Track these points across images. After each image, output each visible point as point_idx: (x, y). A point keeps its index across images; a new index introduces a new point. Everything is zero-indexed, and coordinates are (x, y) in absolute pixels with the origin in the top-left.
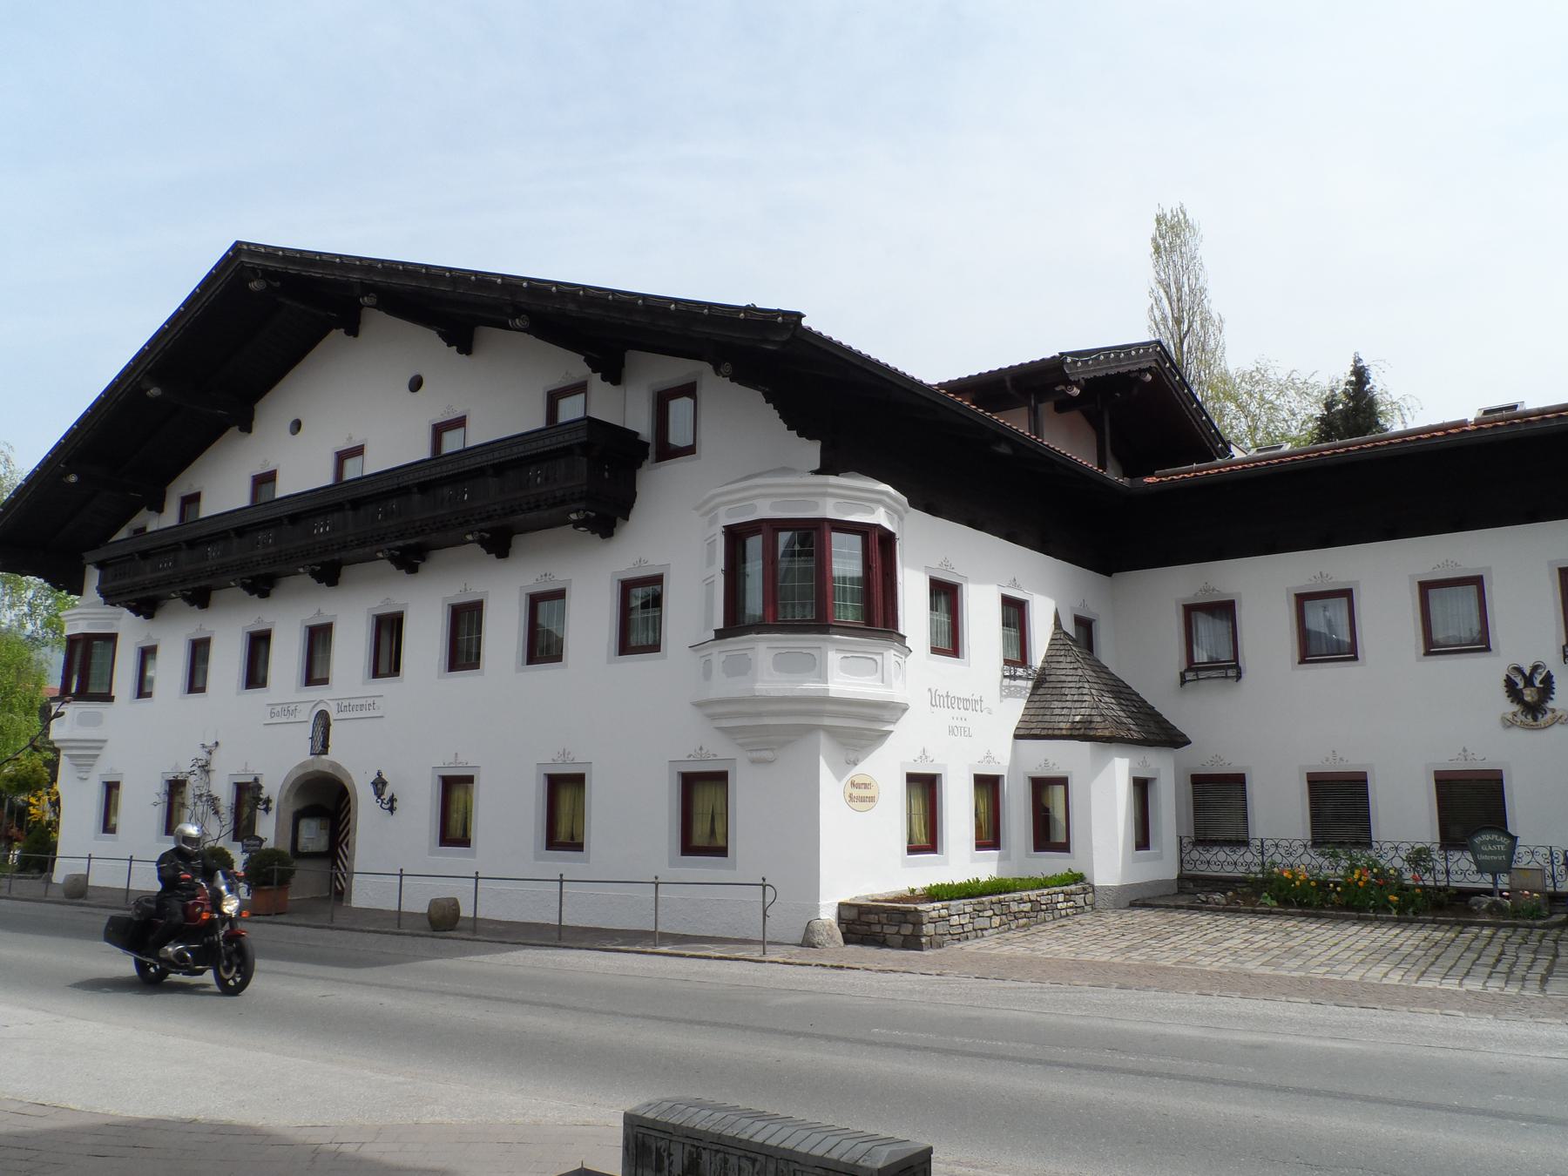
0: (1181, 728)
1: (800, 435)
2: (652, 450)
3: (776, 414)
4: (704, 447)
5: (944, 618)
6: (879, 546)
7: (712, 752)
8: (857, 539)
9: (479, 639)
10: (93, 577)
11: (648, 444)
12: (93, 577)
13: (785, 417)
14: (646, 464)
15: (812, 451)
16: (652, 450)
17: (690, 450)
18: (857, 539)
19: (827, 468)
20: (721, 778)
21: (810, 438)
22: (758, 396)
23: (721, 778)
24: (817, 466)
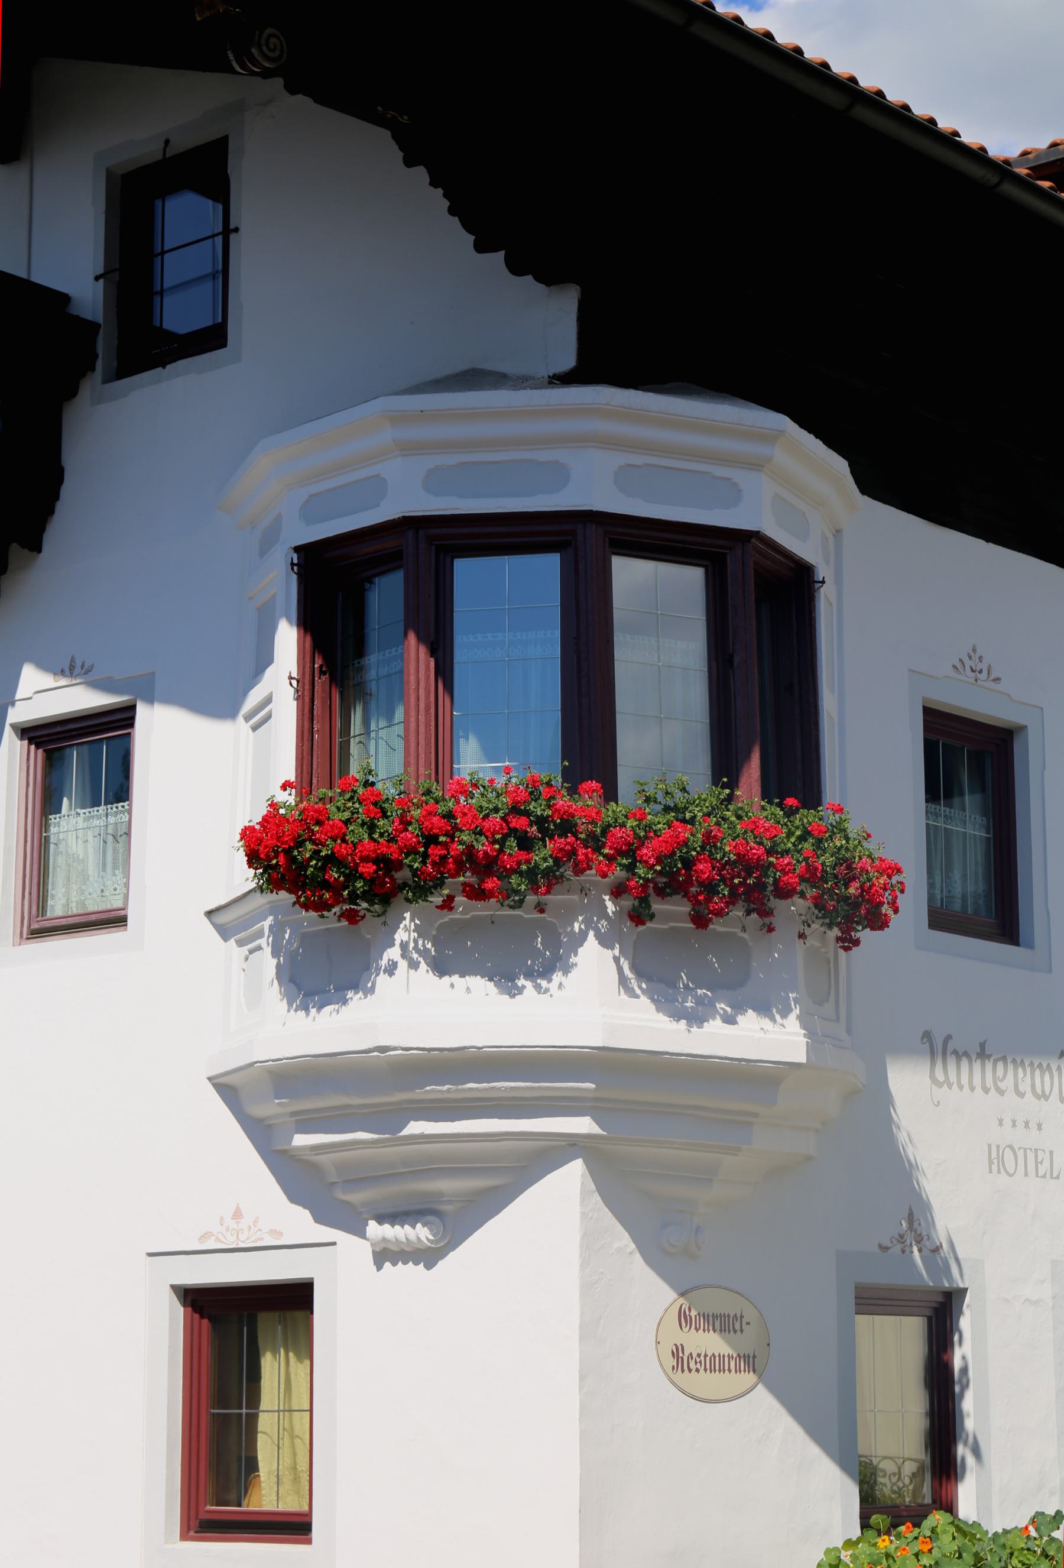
0: (222, 135)
1: (516, 267)
2: (104, 346)
3: (438, 201)
4: (244, 327)
5: (969, 824)
6: (765, 612)
7: (259, 1231)
8: (690, 579)
9: (931, 886)
10: (258, 827)
11: (94, 327)
12: (258, 827)
13: (464, 209)
14: (91, 386)
15: (549, 321)
16: (104, 346)
17: (212, 338)
18: (690, 579)
19: (595, 366)
20: (296, 1298)
21: (550, 277)
22: (382, 144)
23: (296, 1298)
24: (568, 361)
